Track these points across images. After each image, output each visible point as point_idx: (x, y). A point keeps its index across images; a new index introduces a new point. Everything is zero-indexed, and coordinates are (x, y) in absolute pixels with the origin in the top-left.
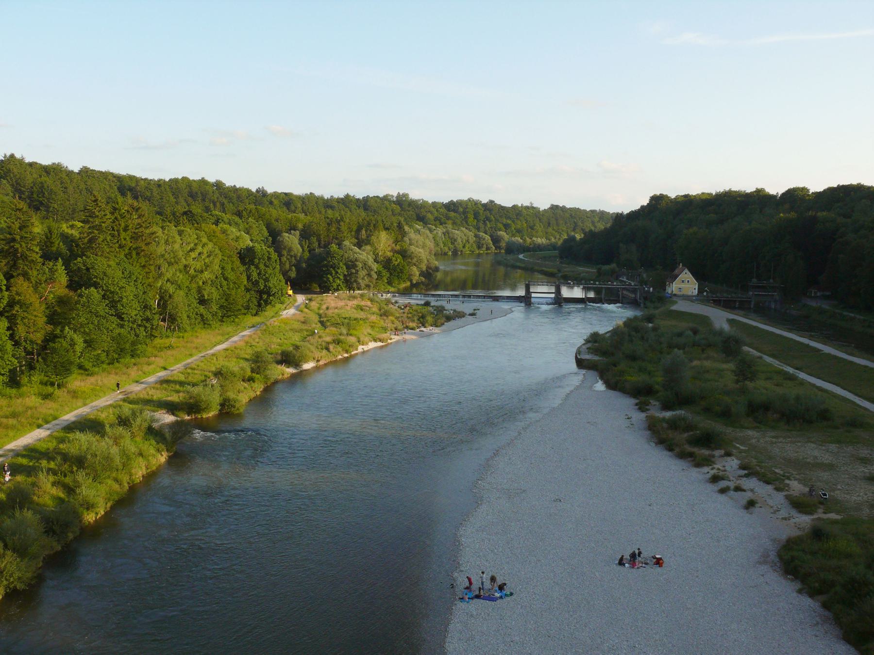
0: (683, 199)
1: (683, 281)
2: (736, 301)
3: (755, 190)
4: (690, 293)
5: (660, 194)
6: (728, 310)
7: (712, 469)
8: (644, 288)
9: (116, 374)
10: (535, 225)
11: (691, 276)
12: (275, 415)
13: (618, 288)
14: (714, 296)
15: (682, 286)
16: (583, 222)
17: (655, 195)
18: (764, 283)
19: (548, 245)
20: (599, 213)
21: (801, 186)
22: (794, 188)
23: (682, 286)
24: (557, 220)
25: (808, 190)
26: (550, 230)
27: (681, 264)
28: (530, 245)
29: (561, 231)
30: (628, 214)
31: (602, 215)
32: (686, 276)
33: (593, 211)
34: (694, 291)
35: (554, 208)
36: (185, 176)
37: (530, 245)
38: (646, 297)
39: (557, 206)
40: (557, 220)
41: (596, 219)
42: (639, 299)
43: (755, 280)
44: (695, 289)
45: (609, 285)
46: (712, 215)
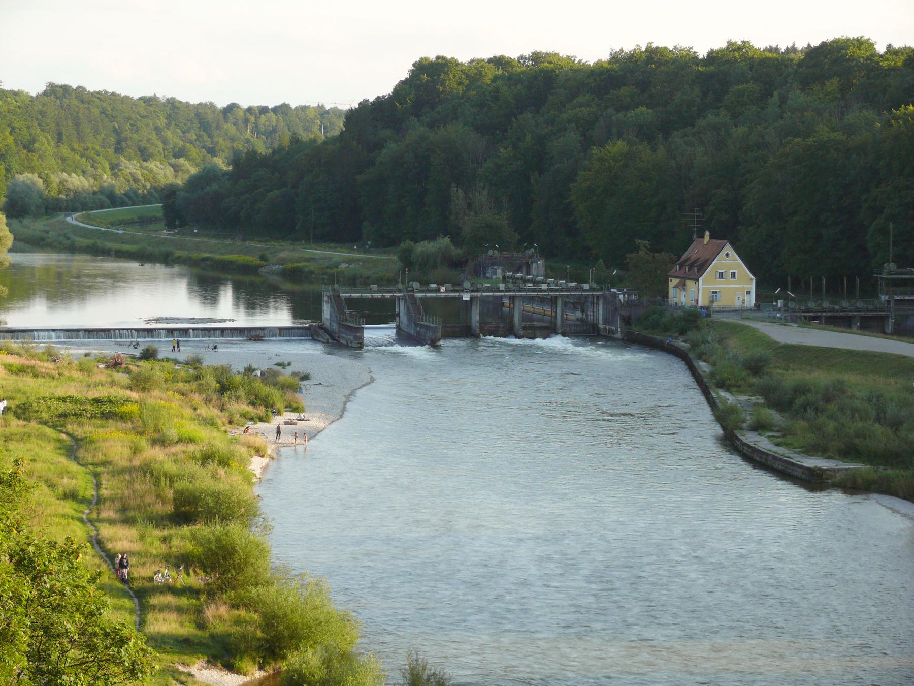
0: (491, 72)
1: (721, 275)
2: (556, 297)
3: (724, 45)
4: (738, 304)
5: (438, 58)
6: (906, 339)
7: (881, 661)
8: (615, 296)
9: (168, 529)
10: (34, 141)
11: (740, 261)
12: (292, 612)
13: (501, 297)
14: (837, 307)
15: (719, 286)
16: (136, 129)
17: (732, 48)
18: (541, 290)
19: (94, 193)
20: (164, 105)
21: (852, 34)
22: (836, 41)
23: (719, 286)
24: (77, 124)
25: (870, 45)
26: (65, 150)
27: (707, 233)
28: (60, 192)
29: (92, 154)
30: (373, 103)
31: (322, 112)
32: (728, 261)
33: (149, 101)
34: (747, 297)
35: (56, 92)
36: (60, 81)
37: (60, 192)
38: (629, 317)
39: (65, 89)
40: (77, 124)
41: (162, 122)
42: (606, 321)
43: (892, 266)
44: (749, 293)
45: (529, 290)
46: (643, 109)
